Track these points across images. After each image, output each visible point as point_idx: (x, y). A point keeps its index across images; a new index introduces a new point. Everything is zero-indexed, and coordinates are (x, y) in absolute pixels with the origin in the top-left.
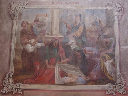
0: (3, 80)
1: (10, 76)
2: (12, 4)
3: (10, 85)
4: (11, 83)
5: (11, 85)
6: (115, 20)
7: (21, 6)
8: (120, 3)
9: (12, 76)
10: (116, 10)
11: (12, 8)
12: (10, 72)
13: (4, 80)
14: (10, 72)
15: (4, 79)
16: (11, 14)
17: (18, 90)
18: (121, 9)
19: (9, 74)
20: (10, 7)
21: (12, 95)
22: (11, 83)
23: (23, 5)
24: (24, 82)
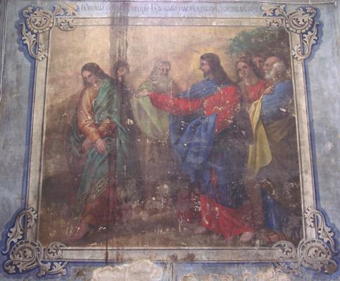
0: (316, 38)
1: (28, 222)
2: (29, 14)
3: (28, 248)
4: (32, 243)
5: (31, 249)
6: (293, 56)
7: (57, 19)
8: (309, 10)
9: (295, 48)
10: (297, 28)
11: (30, 26)
12: (30, 211)
13: (11, 232)
14: (300, 58)
15: (11, 230)
16: (27, 42)
17: (52, 265)
18: (312, 25)
19: (303, 54)
20: (26, 22)
21: (36, 280)
22: (32, 243)
23: (62, 13)
24: (203, 102)
